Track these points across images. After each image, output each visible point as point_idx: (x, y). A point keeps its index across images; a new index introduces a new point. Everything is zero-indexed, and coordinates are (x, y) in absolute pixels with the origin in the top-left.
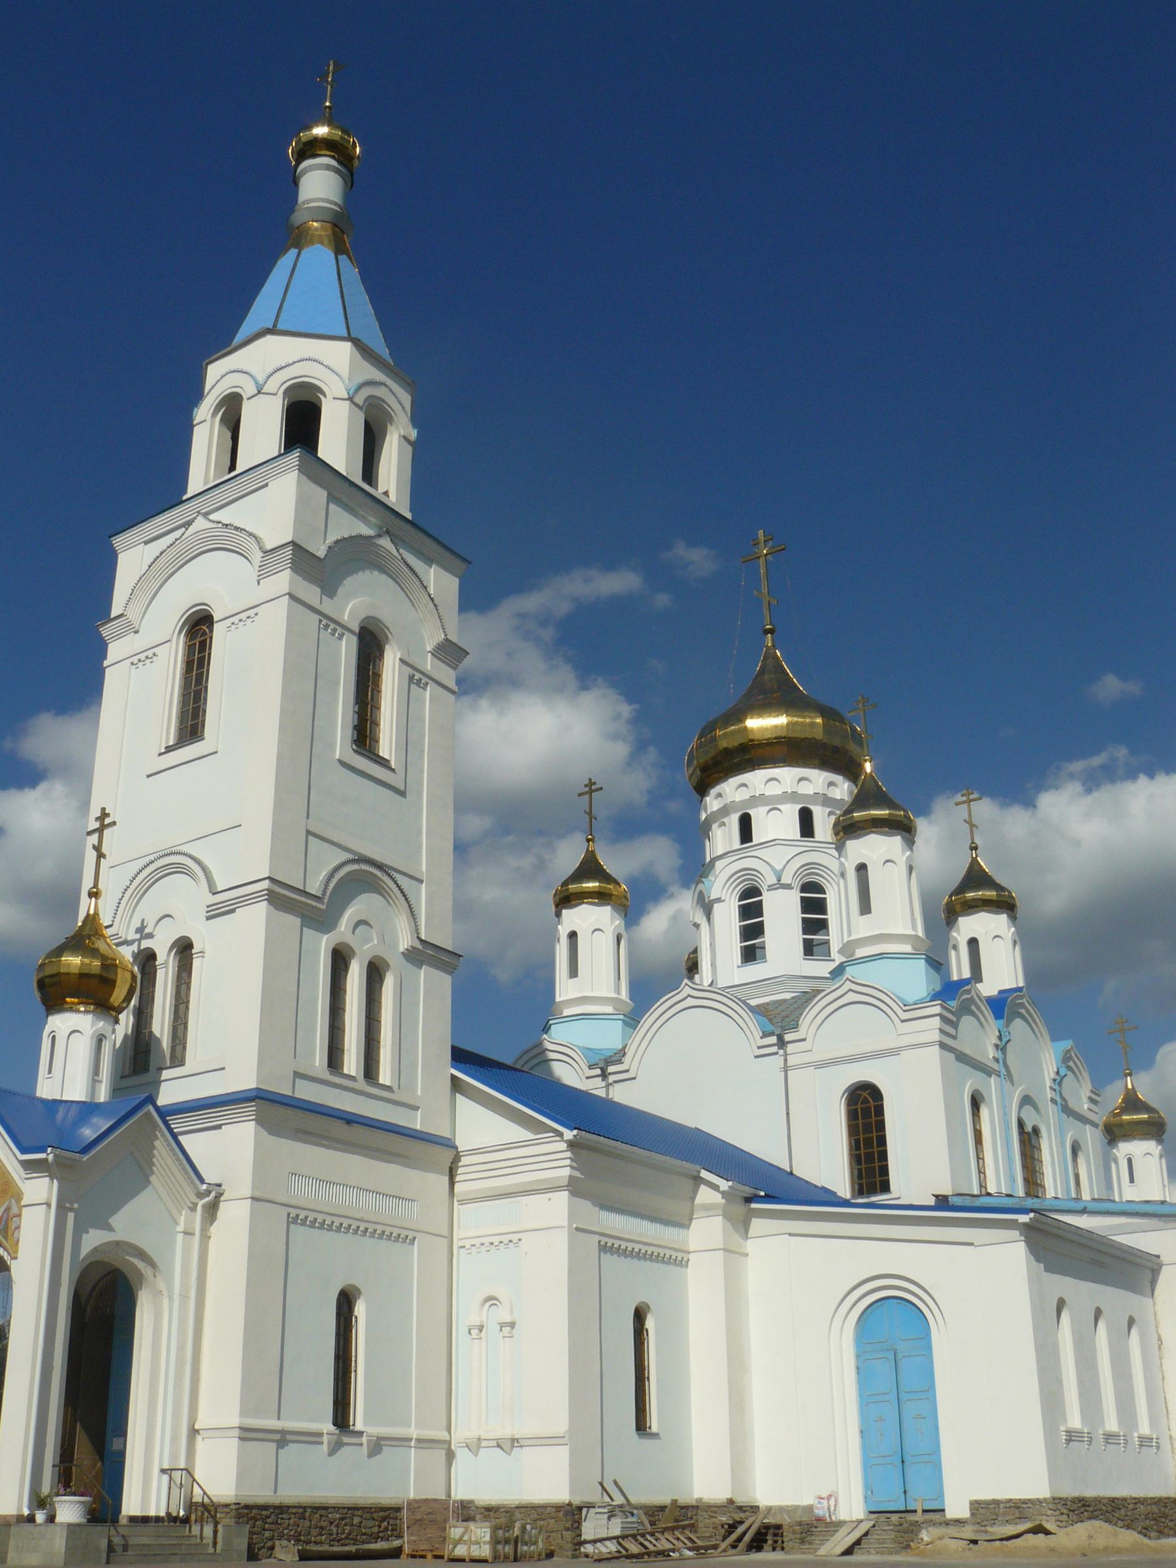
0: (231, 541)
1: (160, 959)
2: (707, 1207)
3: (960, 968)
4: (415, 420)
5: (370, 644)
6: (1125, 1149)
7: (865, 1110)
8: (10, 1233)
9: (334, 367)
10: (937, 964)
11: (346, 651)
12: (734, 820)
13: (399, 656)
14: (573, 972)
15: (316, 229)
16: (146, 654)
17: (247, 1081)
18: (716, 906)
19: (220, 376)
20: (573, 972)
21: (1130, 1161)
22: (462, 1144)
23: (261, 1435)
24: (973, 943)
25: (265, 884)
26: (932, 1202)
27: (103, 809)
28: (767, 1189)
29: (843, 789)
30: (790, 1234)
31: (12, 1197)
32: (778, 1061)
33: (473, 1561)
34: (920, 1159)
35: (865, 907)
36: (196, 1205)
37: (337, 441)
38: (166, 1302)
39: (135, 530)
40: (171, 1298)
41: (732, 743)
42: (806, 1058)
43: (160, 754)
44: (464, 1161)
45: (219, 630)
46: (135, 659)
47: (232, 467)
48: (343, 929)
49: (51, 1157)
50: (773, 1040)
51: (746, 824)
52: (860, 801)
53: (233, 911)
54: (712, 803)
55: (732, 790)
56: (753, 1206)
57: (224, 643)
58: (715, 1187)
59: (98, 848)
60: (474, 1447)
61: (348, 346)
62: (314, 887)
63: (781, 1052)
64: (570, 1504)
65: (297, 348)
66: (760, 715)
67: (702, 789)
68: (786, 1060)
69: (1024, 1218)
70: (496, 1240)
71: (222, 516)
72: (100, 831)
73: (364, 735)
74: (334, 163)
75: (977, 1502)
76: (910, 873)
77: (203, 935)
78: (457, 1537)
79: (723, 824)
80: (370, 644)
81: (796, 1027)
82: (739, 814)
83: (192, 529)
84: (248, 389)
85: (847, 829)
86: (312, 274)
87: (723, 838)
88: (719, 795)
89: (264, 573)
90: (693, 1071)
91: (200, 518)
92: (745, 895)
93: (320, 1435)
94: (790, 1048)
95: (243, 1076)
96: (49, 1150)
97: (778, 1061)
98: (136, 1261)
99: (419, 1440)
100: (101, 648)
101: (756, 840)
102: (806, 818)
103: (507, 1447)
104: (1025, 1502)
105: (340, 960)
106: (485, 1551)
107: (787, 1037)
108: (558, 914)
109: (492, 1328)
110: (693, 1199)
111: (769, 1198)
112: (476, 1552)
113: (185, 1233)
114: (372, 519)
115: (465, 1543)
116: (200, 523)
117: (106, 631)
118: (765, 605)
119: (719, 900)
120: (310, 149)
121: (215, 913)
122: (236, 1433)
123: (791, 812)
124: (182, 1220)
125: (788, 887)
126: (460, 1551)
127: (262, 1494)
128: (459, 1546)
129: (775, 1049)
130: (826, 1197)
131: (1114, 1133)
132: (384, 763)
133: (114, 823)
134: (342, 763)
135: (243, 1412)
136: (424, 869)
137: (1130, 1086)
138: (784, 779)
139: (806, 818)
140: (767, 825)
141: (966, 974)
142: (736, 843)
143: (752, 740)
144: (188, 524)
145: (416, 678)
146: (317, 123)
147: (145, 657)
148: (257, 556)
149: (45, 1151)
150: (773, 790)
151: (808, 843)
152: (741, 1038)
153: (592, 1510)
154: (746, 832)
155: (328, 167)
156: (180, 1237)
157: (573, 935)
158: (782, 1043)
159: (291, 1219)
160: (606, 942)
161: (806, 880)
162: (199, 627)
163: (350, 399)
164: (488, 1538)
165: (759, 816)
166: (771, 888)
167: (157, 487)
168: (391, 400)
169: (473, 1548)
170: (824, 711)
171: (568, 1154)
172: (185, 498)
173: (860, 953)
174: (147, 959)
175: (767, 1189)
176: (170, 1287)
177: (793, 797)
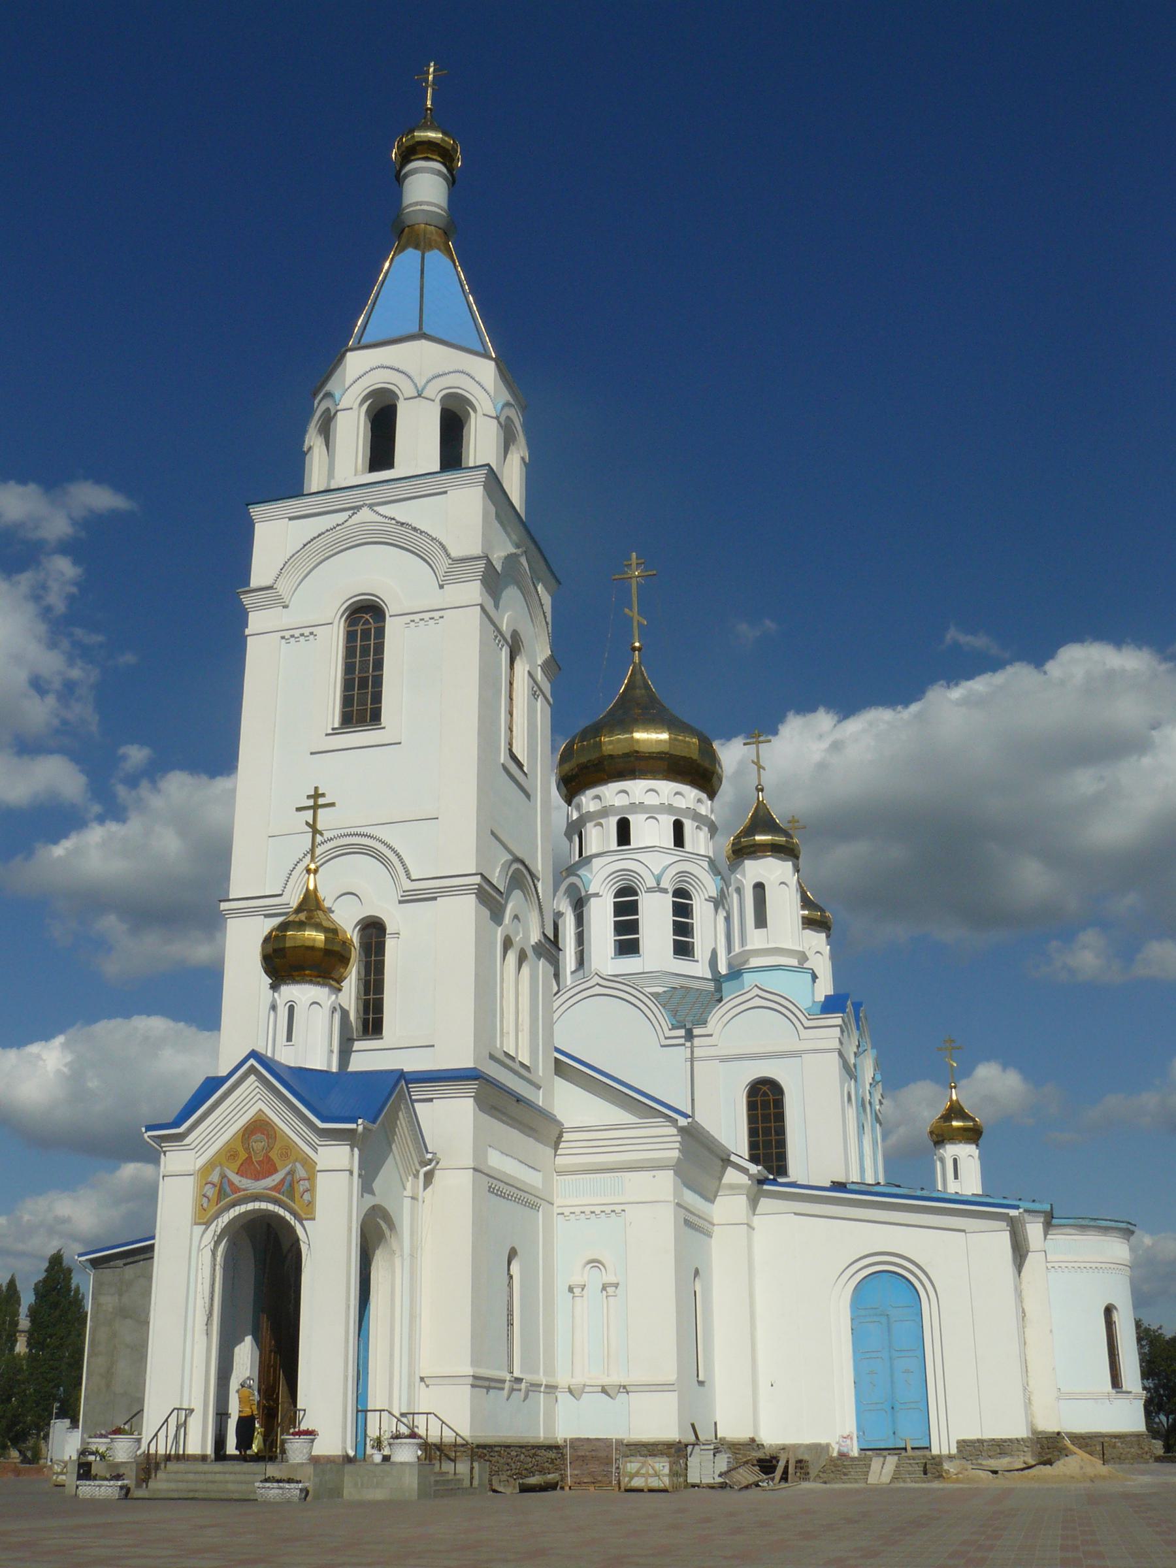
0: (407, 539)
2: (732, 1187)
7: (766, 1102)
8: (297, 1196)
12: (612, 823)
13: (527, 669)
15: (432, 233)
16: (301, 631)
17: (465, 1061)
18: (592, 899)
19: (359, 372)
21: (955, 1161)
23: (660, 1388)
26: (828, 1184)
27: (316, 788)
30: (795, 1214)
31: (296, 1160)
32: (684, 1052)
33: (651, 1491)
35: (761, 921)
36: (418, 1172)
38: (398, 1262)
39: (280, 504)
40: (402, 1256)
41: (618, 750)
42: (712, 1052)
43: (327, 735)
44: (566, 1136)
46: (287, 634)
49: (360, 1128)
50: (682, 1032)
53: (435, 899)
56: (765, 1187)
57: (398, 641)
58: (745, 1171)
63: (688, 1044)
64: (680, 1442)
65: (421, 354)
66: (646, 730)
68: (692, 1052)
70: (608, 1209)
74: (444, 170)
75: (964, 1441)
77: (394, 918)
78: (633, 1471)
79: (601, 825)
81: (705, 1023)
82: (617, 818)
83: (356, 519)
84: (405, 388)
87: (601, 837)
88: (598, 797)
91: (365, 509)
92: (620, 893)
93: (504, 1381)
94: (696, 1041)
96: (360, 1121)
97: (684, 1052)
98: (382, 1223)
99: (547, 1386)
100: (241, 617)
101: (635, 842)
104: (1005, 1441)
106: (666, 1482)
107: (696, 1032)
110: (720, 1179)
112: (654, 1483)
113: (413, 1198)
114: (514, 537)
115: (643, 1475)
117: (246, 600)
118: (635, 624)
119: (597, 895)
121: (407, 899)
122: (470, 1381)
123: (667, 821)
124: (409, 1185)
125: (665, 891)
126: (637, 1483)
127: (490, 1435)
128: (636, 1479)
129: (682, 1041)
133: (332, 805)
135: (475, 1362)
136: (540, 868)
137: (954, 1098)
139: (678, 827)
140: (646, 832)
142: (613, 844)
143: (637, 752)
144: (357, 508)
147: (305, 633)
148: (443, 564)
149: (354, 1121)
150: (651, 800)
151: (678, 852)
153: (697, 1447)
154: (624, 832)
155: (439, 173)
156: (407, 1202)
158: (689, 1036)
159: (494, 1187)
161: (677, 886)
163: (497, 418)
164: (666, 1471)
166: (650, 890)
169: (650, 1480)
171: (679, 1138)
173: (754, 962)
176: (402, 1249)
177: (669, 809)
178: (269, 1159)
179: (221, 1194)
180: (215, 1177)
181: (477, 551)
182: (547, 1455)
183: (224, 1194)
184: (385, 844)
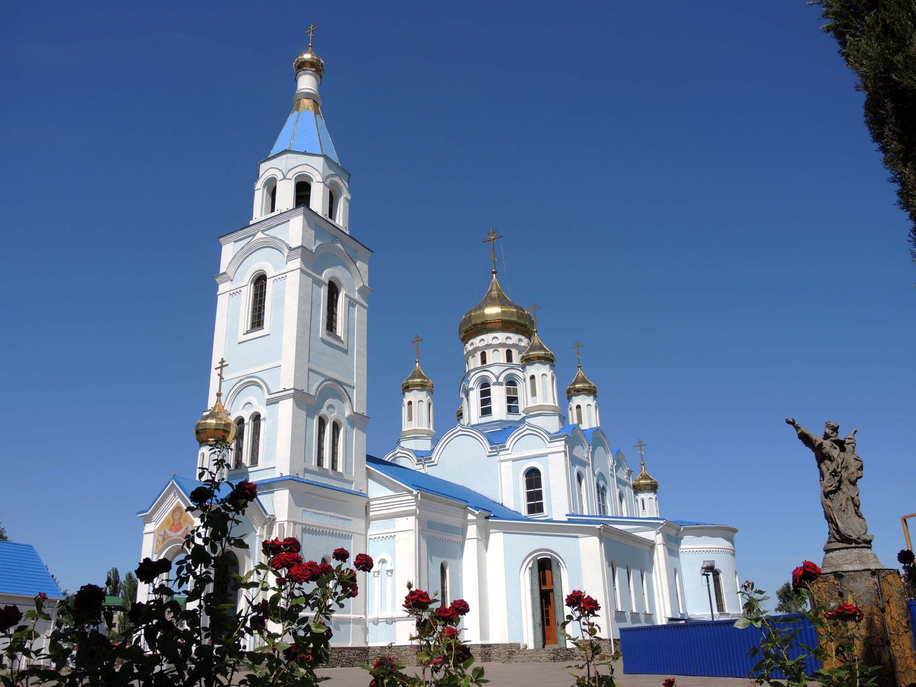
0: (273, 245)
1: (246, 421)
2: (472, 521)
3: (573, 419)
4: (350, 191)
5: (333, 290)
6: (641, 496)
7: (533, 477)
9: (315, 169)
10: (563, 419)
11: (324, 292)
12: (478, 354)
14: (410, 419)
19: (267, 170)
20: (410, 419)
22: (371, 496)
24: (578, 407)
25: (292, 391)
28: (492, 514)
29: (525, 342)
34: (557, 502)
35: (534, 394)
37: (318, 201)
45: (269, 282)
47: (273, 210)
48: (324, 411)
51: (483, 355)
52: (533, 348)
54: (469, 347)
55: (477, 342)
59: (220, 375)
60: (376, 622)
61: (322, 159)
62: (313, 393)
65: (298, 157)
67: (465, 339)
69: (598, 526)
70: (385, 536)
71: (270, 232)
72: (221, 367)
73: (331, 325)
76: (621, 501)
77: (264, 412)
80: (333, 290)
85: (527, 361)
86: (303, 125)
87: (475, 362)
89: (289, 258)
90: (460, 460)
95: (283, 468)
102: (509, 353)
103: (390, 621)
105: (322, 423)
108: (404, 394)
109: (384, 573)
111: (495, 517)
116: (260, 235)
120: (302, 66)
121: (270, 402)
123: (503, 351)
125: (501, 384)
130: (515, 516)
131: (637, 489)
132: (338, 338)
134: (323, 340)
138: (501, 337)
139: (509, 353)
140: (491, 358)
141: (576, 422)
142: (479, 364)
144: (254, 235)
145: (351, 303)
146: (306, 52)
148: (286, 252)
150: (496, 342)
152: (478, 447)
157: (410, 403)
160: (424, 406)
162: (260, 281)
165: (489, 353)
166: (494, 384)
167: (239, 219)
168: (342, 184)
170: (516, 307)
172: (251, 222)
174: (241, 421)
175: (492, 514)
178: (180, 523)
179: (164, 539)
180: (162, 533)
181: (299, 244)
182: (490, 646)
183: (165, 537)
184: (263, 381)
